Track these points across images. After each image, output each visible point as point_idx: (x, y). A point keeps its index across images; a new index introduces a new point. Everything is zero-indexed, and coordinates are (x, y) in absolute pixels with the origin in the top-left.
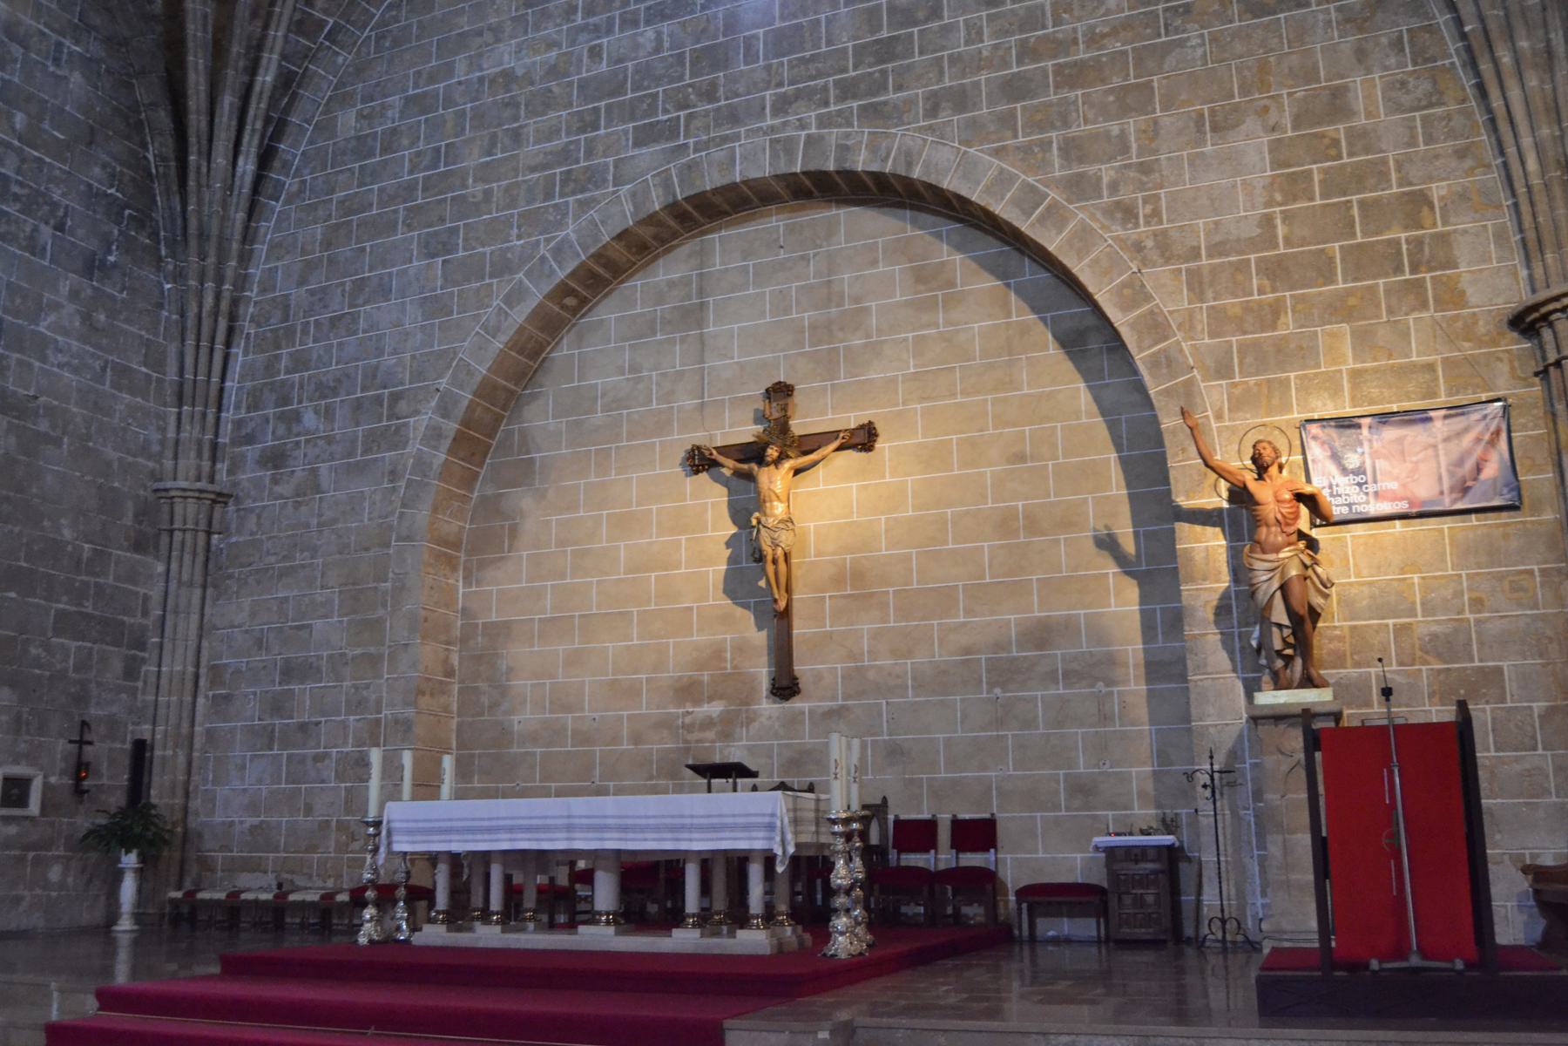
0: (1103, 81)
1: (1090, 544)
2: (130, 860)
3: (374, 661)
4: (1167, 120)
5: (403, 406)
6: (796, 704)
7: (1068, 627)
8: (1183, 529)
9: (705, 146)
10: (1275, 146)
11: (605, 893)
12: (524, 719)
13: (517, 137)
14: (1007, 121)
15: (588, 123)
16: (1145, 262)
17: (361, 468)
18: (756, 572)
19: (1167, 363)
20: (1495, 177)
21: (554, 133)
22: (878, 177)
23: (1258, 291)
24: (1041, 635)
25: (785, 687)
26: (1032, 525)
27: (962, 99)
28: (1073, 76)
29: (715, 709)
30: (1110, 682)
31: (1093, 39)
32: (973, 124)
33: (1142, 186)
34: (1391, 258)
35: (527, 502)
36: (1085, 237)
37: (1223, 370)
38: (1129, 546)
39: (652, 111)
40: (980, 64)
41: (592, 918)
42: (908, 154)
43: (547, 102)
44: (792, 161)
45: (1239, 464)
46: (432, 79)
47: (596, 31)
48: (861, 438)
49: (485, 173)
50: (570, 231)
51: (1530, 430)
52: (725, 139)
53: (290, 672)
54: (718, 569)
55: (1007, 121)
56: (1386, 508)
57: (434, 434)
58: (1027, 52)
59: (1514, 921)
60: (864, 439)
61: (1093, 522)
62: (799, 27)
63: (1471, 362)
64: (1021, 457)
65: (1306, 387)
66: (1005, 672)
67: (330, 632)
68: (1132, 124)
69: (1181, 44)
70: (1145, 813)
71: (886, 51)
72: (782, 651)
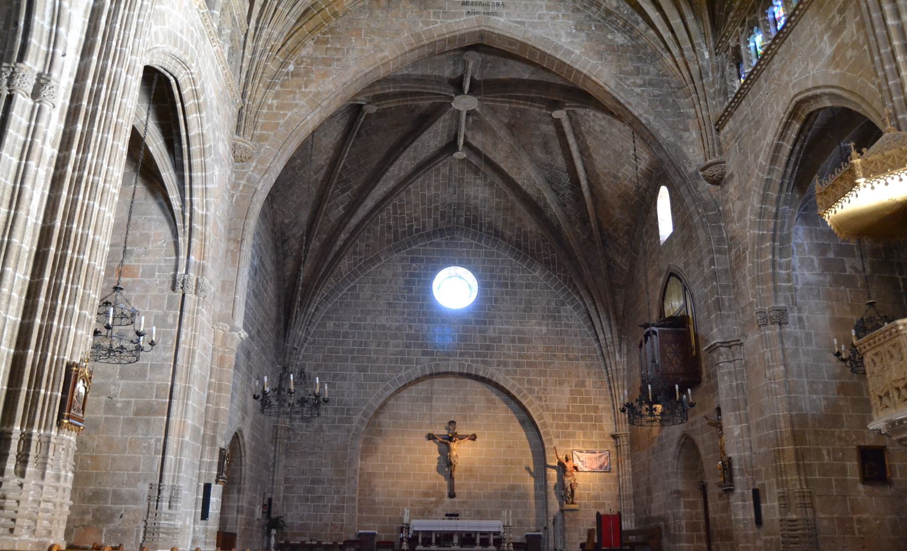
2: (274, 532)
3: (343, 481)
5: (351, 412)
6: (454, 499)
7: (519, 486)
8: (548, 469)
10: (571, 390)
12: (379, 498)
13: (387, 344)
14: (515, 372)
17: (338, 427)
18: (447, 465)
19: (547, 433)
20: (610, 405)
24: (513, 488)
25: (452, 495)
28: (531, 365)
29: (433, 499)
31: (535, 357)
32: (508, 371)
34: (591, 419)
35: (380, 441)
36: (531, 403)
37: (558, 437)
38: (532, 470)
40: (509, 356)
43: (396, 337)
45: (562, 458)
46: (359, 320)
47: (411, 321)
49: (376, 352)
50: (403, 374)
51: (613, 457)
53: (313, 482)
58: (520, 356)
60: (473, 438)
61: (525, 464)
66: (504, 496)
67: (327, 471)
68: (542, 379)
70: (533, 528)
71: (488, 348)
72: (451, 487)
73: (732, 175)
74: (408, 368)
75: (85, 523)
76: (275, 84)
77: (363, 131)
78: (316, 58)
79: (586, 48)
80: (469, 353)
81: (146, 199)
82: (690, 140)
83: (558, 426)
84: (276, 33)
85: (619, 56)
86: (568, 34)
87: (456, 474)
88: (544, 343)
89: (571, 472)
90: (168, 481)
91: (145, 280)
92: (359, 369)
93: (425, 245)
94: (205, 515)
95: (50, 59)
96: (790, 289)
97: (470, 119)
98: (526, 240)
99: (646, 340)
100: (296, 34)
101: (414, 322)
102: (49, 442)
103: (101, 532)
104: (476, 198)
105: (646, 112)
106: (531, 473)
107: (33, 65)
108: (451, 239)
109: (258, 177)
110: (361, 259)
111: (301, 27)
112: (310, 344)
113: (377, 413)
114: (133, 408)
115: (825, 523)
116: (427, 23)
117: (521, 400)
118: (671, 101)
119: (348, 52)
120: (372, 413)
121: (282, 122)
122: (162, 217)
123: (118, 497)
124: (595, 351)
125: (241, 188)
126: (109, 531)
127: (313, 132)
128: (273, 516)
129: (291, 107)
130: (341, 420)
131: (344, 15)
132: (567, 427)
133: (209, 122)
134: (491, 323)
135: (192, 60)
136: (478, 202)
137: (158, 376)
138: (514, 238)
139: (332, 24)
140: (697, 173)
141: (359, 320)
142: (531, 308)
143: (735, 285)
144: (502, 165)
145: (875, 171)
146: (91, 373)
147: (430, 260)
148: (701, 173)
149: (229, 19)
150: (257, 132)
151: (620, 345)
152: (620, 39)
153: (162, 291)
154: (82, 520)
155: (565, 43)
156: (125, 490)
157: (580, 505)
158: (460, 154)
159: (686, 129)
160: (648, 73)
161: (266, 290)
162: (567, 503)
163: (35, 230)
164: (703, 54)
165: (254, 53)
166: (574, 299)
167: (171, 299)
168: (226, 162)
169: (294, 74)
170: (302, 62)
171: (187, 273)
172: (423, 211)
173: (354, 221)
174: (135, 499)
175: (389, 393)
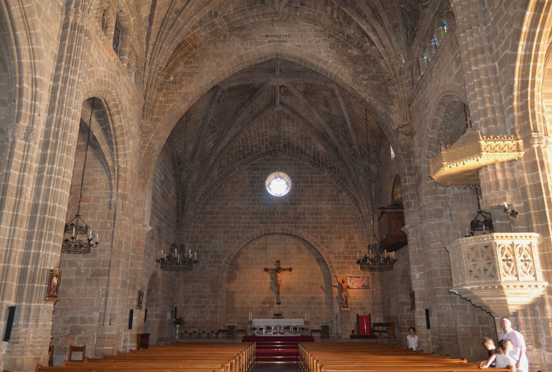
2: (178, 326)
5: (221, 257)
6: (280, 305)
12: (237, 306)
13: (240, 218)
18: (276, 284)
19: (332, 267)
21: (246, 219)
23: (343, 260)
26: (312, 284)
27: (308, 228)
28: (322, 228)
29: (268, 305)
31: (325, 223)
35: (238, 273)
37: (338, 269)
46: (225, 204)
50: (249, 235)
51: (370, 280)
53: (200, 297)
55: (313, 232)
56: (355, 287)
57: (227, 263)
58: (316, 223)
60: (290, 270)
68: (329, 236)
71: (297, 218)
73: (416, 132)
74: (252, 231)
75: (66, 335)
76: (163, 89)
77: (221, 99)
78: (185, 73)
79: (336, 59)
80: (286, 222)
81: (94, 159)
82: (394, 110)
83: (338, 263)
84: (162, 60)
85: (354, 62)
86: (325, 51)
87: (281, 290)
88: (330, 215)
89: (346, 289)
90: (109, 312)
91: (95, 204)
92: (225, 233)
93: (261, 160)
94: (130, 327)
95: (32, 120)
96: (445, 198)
97: (282, 89)
98: (318, 155)
99: (382, 216)
100: (174, 59)
101: (256, 204)
102: (39, 309)
103: (74, 339)
104: (289, 132)
105: (369, 95)
106: (323, 289)
107: (24, 123)
108: (276, 156)
109: (155, 142)
110: (225, 170)
111: (176, 55)
112: (197, 219)
113: (236, 257)
114: (90, 273)
115: (463, 330)
116: (246, 49)
117: (317, 248)
118: (384, 87)
119: (202, 68)
120: (232, 257)
121: (167, 110)
122: (103, 169)
123: (83, 320)
124: (359, 219)
125: (146, 148)
126: (78, 338)
127: (186, 113)
128: (178, 317)
129: (172, 101)
130: (215, 262)
131: (200, 46)
132: (344, 263)
133: (126, 118)
134: (299, 204)
135: (112, 89)
136: (290, 135)
137: (103, 255)
138: (312, 155)
139: (194, 52)
140: (398, 129)
141: (225, 204)
142: (322, 195)
143: (418, 194)
144: (302, 114)
145: (453, 159)
146: (60, 273)
147: (264, 169)
148: (400, 129)
149: (134, 58)
150: (155, 116)
151: (373, 215)
152: (355, 52)
153: (104, 209)
154: (64, 333)
155: (324, 57)
156: (86, 316)
157: (351, 308)
158: (279, 108)
159: (392, 104)
160: (371, 72)
161: (170, 192)
162: (344, 307)
163: (29, 206)
164: (402, 60)
165: (150, 73)
166: (347, 189)
167: (109, 214)
168: (137, 136)
169: (174, 82)
170: (178, 75)
171: (117, 199)
172: (259, 141)
173: (219, 149)
174: (92, 320)
175: (241, 246)
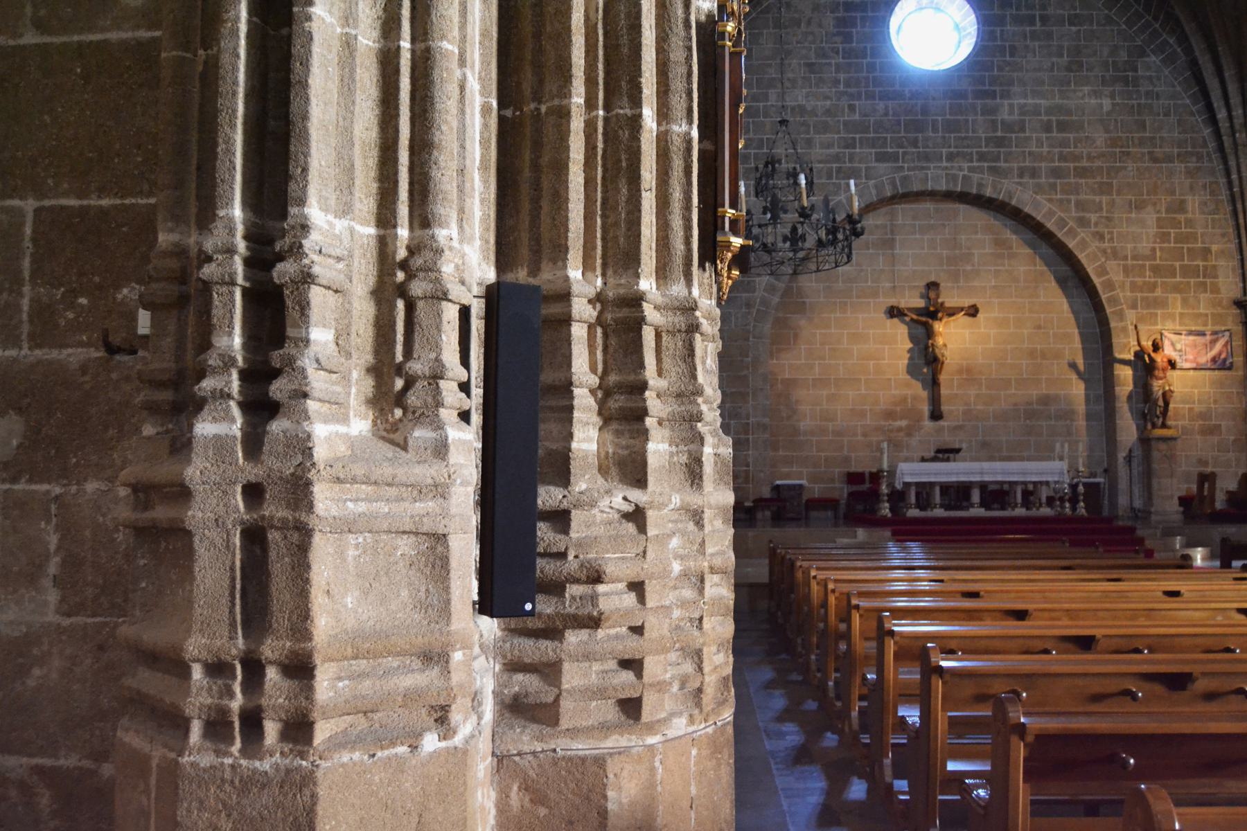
0: (1094, 178)
1: (1066, 367)
4: (1118, 200)
6: (941, 423)
7: (1056, 398)
8: (1117, 366)
9: (913, 169)
10: (1158, 219)
11: (976, 496)
12: (805, 424)
15: (850, 144)
16: (1107, 259)
19: (1114, 301)
21: (830, 146)
22: (1029, 216)
23: (1149, 277)
24: (1046, 400)
25: (936, 415)
27: (1034, 173)
28: (1082, 172)
29: (904, 423)
30: (1072, 420)
31: (1090, 158)
32: (1038, 186)
33: (1107, 227)
34: (1194, 272)
36: (1083, 244)
38: (1081, 367)
39: (884, 145)
41: (972, 506)
42: (1010, 192)
43: (825, 128)
44: (956, 185)
45: (1147, 344)
48: (972, 311)
52: (923, 168)
54: (904, 362)
58: (1062, 158)
59: (1219, 504)
60: (973, 312)
61: (1068, 357)
62: (958, 121)
63: (1220, 315)
64: (1039, 327)
65: (1164, 318)
66: (1031, 414)
68: (1104, 199)
69: (1125, 168)
71: (1000, 142)
72: (935, 400)
